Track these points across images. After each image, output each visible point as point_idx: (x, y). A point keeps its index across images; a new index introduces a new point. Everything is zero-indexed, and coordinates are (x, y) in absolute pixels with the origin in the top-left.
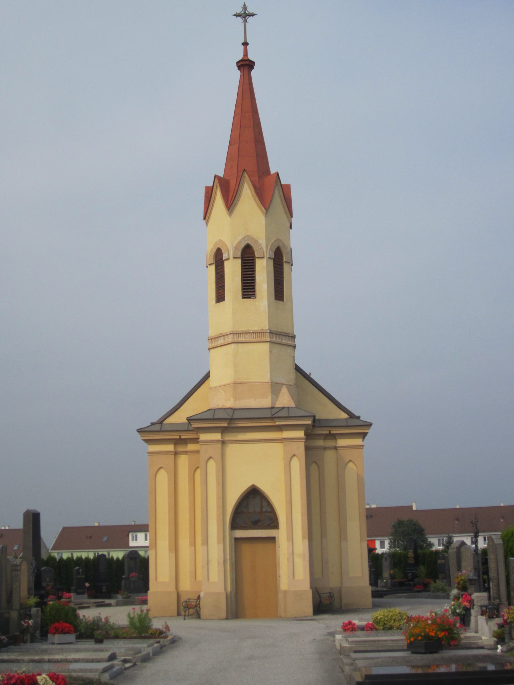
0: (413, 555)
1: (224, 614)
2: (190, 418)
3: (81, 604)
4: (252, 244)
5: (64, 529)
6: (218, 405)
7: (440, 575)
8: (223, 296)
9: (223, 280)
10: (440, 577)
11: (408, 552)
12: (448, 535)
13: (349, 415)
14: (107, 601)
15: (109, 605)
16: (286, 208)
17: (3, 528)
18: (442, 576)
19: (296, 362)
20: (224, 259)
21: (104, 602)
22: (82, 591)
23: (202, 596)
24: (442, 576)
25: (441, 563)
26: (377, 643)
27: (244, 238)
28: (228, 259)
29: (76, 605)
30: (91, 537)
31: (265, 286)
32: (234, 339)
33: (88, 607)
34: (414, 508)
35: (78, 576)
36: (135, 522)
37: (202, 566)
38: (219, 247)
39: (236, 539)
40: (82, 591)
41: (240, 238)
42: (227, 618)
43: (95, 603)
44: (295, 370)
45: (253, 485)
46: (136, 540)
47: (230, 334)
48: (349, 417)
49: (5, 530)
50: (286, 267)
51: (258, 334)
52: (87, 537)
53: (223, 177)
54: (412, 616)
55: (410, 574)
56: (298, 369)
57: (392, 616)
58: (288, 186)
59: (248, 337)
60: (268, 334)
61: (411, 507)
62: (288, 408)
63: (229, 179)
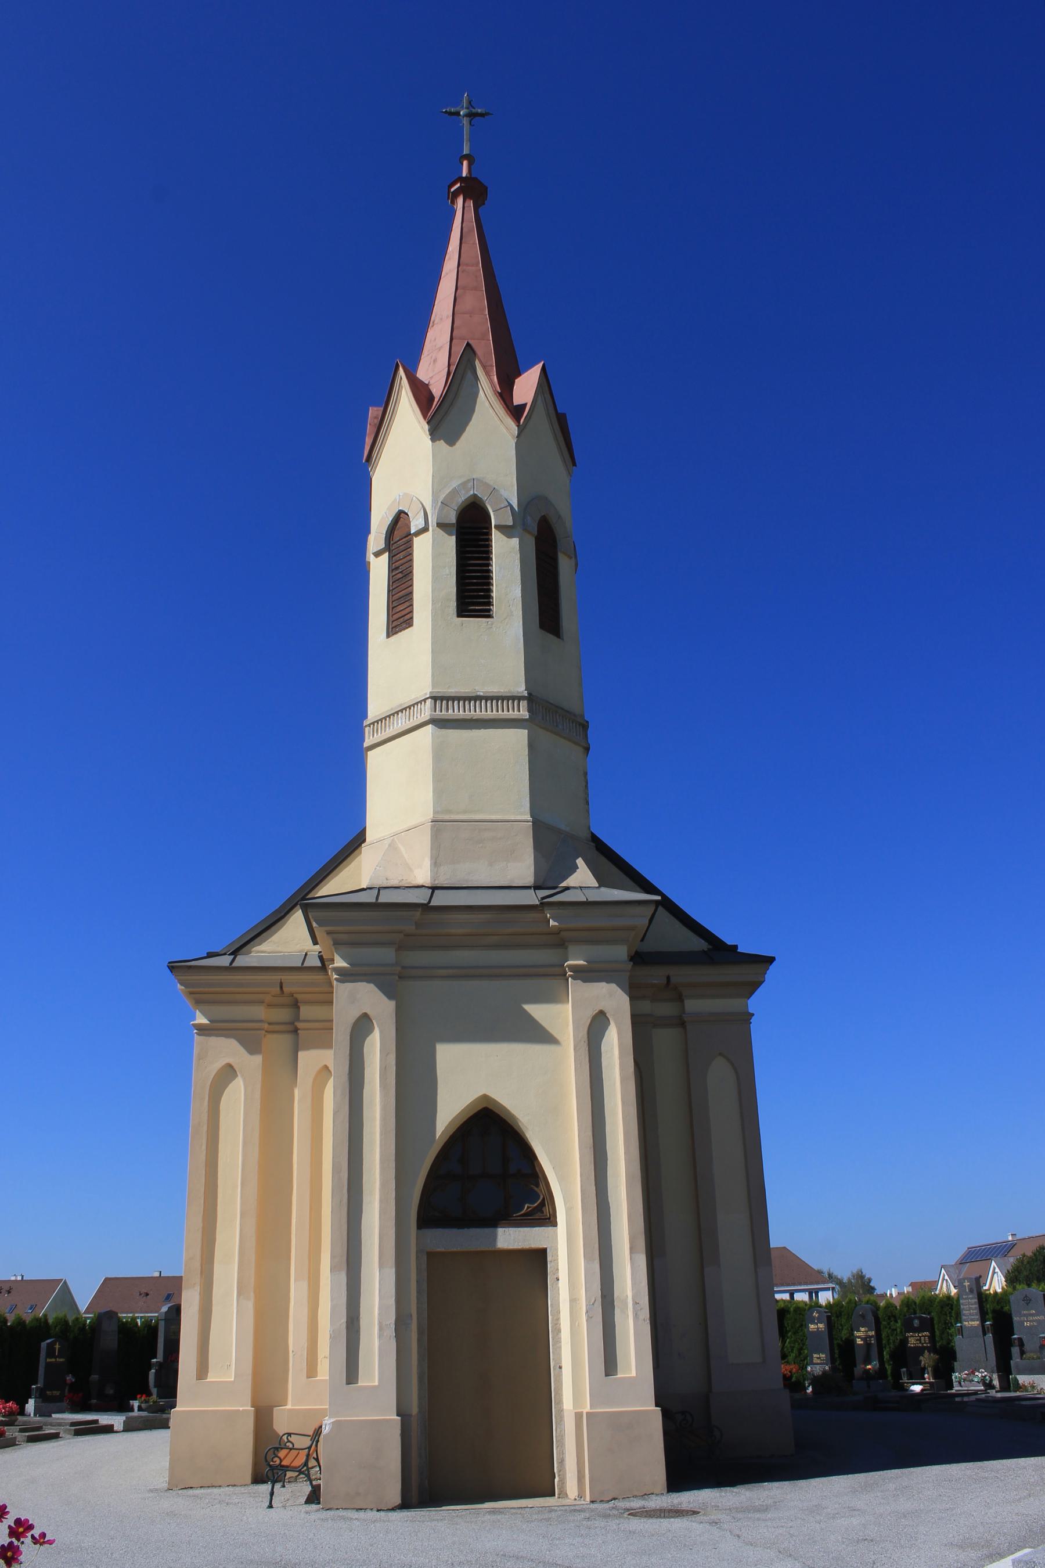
1: (395, 1496)
3: (40, 1428)
4: (483, 495)
5: (107, 1280)
6: (387, 879)
7: (815, 1356)
9: (411, 579)
10: (815, 1361)
14: (104, 1419)
15: (109, 1429)
17: (13, 1278)
18: (818, 1358)
21: (96, 1421)
22: (57, 1393)
23: (326, 1430)
24: (818, 1358)
25: (816, 1330)
27: (464, 484)
28: (425, 530)
29: (22, 1431)
30: (147, 1294)
32: (435, 711)
33: (55, 1436)
35: (48, 1360)
37: (558, 1280)
38: (400, 508)
39: (431, 1256)
40: (57, 1393)
41: (455, 484)
43: (73, 1424)
45: (485, 1097)
47: (425, 700)
48: (710, 947)
49: (16, 1281)
52: (140, 1294)
58: (564, 415)
59: (472, 708)
60: (524, 704)
63: (429, 383)
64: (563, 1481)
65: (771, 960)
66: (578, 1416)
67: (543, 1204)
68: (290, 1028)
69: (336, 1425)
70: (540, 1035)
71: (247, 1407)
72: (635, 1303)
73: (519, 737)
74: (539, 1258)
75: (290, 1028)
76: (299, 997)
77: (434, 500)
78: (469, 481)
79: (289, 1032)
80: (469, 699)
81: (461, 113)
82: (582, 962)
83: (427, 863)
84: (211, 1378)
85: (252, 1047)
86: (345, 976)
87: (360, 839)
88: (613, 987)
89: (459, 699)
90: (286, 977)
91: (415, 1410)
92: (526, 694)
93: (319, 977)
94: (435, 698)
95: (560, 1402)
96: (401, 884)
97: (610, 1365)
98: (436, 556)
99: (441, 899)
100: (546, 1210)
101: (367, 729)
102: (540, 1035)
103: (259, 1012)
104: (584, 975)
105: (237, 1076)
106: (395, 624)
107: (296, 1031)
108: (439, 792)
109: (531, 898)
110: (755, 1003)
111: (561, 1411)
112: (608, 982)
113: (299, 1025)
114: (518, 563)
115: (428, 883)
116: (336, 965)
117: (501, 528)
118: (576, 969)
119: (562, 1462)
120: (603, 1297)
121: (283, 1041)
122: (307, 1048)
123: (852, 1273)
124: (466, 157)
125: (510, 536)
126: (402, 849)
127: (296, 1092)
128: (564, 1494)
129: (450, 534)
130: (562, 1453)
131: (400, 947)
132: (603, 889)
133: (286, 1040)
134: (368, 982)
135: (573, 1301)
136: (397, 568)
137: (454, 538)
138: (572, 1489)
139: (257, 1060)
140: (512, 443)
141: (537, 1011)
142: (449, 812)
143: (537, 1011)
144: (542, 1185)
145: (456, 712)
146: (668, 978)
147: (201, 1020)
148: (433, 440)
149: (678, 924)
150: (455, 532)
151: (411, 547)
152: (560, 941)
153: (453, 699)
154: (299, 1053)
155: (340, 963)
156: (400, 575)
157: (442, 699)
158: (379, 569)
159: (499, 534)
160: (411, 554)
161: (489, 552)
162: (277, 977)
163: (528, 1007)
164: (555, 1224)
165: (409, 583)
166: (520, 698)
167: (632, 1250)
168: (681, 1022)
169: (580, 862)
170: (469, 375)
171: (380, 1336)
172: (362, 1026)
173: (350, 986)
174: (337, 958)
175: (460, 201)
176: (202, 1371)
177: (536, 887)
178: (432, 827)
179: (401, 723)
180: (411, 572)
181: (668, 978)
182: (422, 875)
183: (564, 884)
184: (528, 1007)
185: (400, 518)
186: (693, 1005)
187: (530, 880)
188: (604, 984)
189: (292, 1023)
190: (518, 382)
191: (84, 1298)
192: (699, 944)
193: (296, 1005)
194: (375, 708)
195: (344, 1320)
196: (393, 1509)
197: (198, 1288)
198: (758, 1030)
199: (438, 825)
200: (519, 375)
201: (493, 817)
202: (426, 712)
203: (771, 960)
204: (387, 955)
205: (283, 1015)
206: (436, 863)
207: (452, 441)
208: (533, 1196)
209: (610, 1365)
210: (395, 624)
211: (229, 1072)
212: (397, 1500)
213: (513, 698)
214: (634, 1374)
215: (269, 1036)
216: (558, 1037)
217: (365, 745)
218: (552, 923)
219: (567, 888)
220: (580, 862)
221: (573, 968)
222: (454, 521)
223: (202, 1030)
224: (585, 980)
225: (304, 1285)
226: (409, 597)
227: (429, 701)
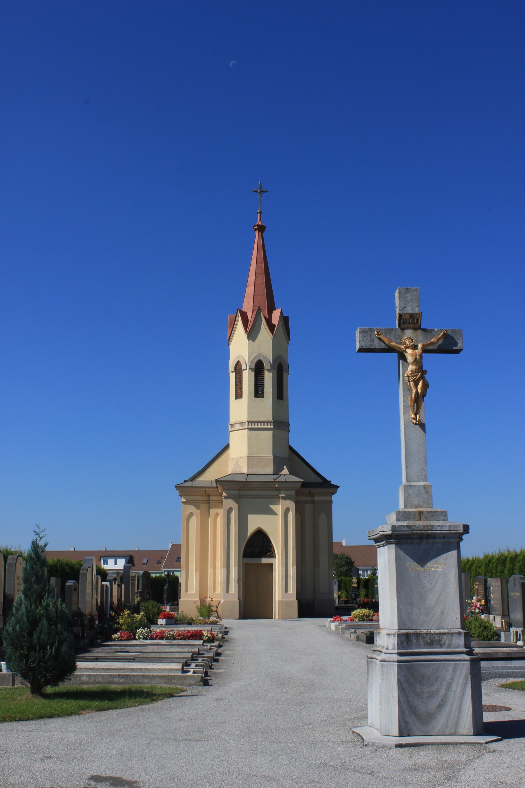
0: (356, 581)
1: (237, 616)
2: (218, 480)
8: (241, 395)
11: (353, 578)
12: (373, 567)
13: (323, 480)
16: (286, 335)
19: (291, 444)
20: (242, 369)
26: (360, 626)
28: (246, 369)
31: (271, 390)
34: (344, 544)
36: (106, 548)
39: (246, 564)
42: (240, 619)
44: (288, 449)
45: (259, 527)
46: (107, 564)
50: (285, 374)
51: (494, 584)
53: (456, 550)
54: (508, 551)
55: (354, 595)
56: (291, 448)
57: (364, 613)
60: (272, 424)
61: (341, 542)
62: (285, 475)
64: (275, 616)
65: (339, 487)
66: (279, 601)
67: (272, 553)
68: (207, 502)
69: (224, 601)
70: (273, 513)
71: (197, 599)
72: (293, 577)
73: (271, 433)
74: (271, 566)
75: (207, 502)
76: (210, 494)
77: (249, 358)
78: (258, 354)
79: (207, 503)
80: (257, 422)
81: (258, 191)
82: (284, 495)
83: (246, 468)
84: (189, 592)
85: (198, 508)
86: (226, 498)
87: (227, 447)
88: (292, 502)
89: (255, 422)
90: (207, 489)
91: (242, 599)
92: (272, 421)
93: (216, 489)
94: (248, 422)
95: (275, 598)
96: (240, 473)
97: (286, 590)
98: (249, 378)
99: (250, 479)
100: (273, 554)
101: (230, 426)
102: (273, 513)
103: (199, 498)
104: (284, 498)
105: (193, 515)
106: (237, 395)
107: (209, 503)
108: (249, 448)
109: (271, 478)
110: (334, 498)
111: (275, 600)
112: (290, 500)
113: (210, 502)
114: (271, 380)
115: (246, 473)
116: (224, 495)
117: (267, 370)
118: (282, 497)
119: (275, 611)
120: (285, 575)
121: (205, 506)
122: (212, 508)
123: (521, 550)
124: (258, 213)
125: (269, 372)
126: (240, 462)
127: (209, 520)
128: (275, 618)
129: (253, 371)
130: (275, 609)
131: (239, 490)
132: (290, 475)
133: (206, 505)
134: (232, 499)
135: (279, 576)
136: (238, 378)
137: (254, 372)
138: (277, 617)
139: (199, 511)
140: (271, 341)
141: (273, 507)
142: (252, 454)
143: (273, 507)
144: (273, 548)
145: (254, 426)
146: (310, 491)
147: (184, 500)
148: (248, 340)
149: (314, 474)
150: (254, 371)
151: (242, 373)
152: (279, 489)
153: (253, 422)
154: (210, 510)
155: (225, 494)
156: (239, 381)
157: (250, 422)
158: (233, 377)
159: (266, 371)
160: (242, 375)
161: (264, 377)
162: (204, 489)
163: (270, 506)
164: (275, 558)
165: (241, 395)
166: (271, 422)
167: (293, 565)
168: (313, 502)
169: (285, 467)
170: (259, 317)
171: (234, 582)
172: (230, 510)
173: (227, 500)
174: (224, 493)
175: (257, 232)
176: (187, 590)
177: (274, 474)
178: (247, 458)
179: (239, 427)
180: (242, 381)
181: (310, 491)
182: (245, 471)
183: (280, 473)
184: (270, 506)
185: (238, 364)
186: (317, 498)
187: (272, 473)
188: (289, 501)
189: (208, 501)
190: (274, 312)
191: (47, 560)
192: (320, 480)
193: (209, 496)
194: (232, 420)
195: (226, 579)
196: (237, 619)
197: (185, 570)
198: (334, 505)
199: (249, 458)
200: (275, 309)
201: (263, 456)
202: (246, 426)
203: (339, 487)
204: (236, 492)
205: (205, 498)
206: (248, 468)
207: (254, 340)
208: (270, 551)
209: (286, 590)
210: (237, 395)
211: (191, 514)
212: (238, 618)
213: (269, 422)
214: (292, 592)
215: (202, 504)
216: (277, 513)
217: (229, 430)
218: (277, 486)
219: (281, 475)
220: (285, 467)
221: (281, 497)
222: (254, 368)
223: (184, 503)
224: (284, 500)
225: (212, 570)
226: (241, 388)
227: (247, 423)
